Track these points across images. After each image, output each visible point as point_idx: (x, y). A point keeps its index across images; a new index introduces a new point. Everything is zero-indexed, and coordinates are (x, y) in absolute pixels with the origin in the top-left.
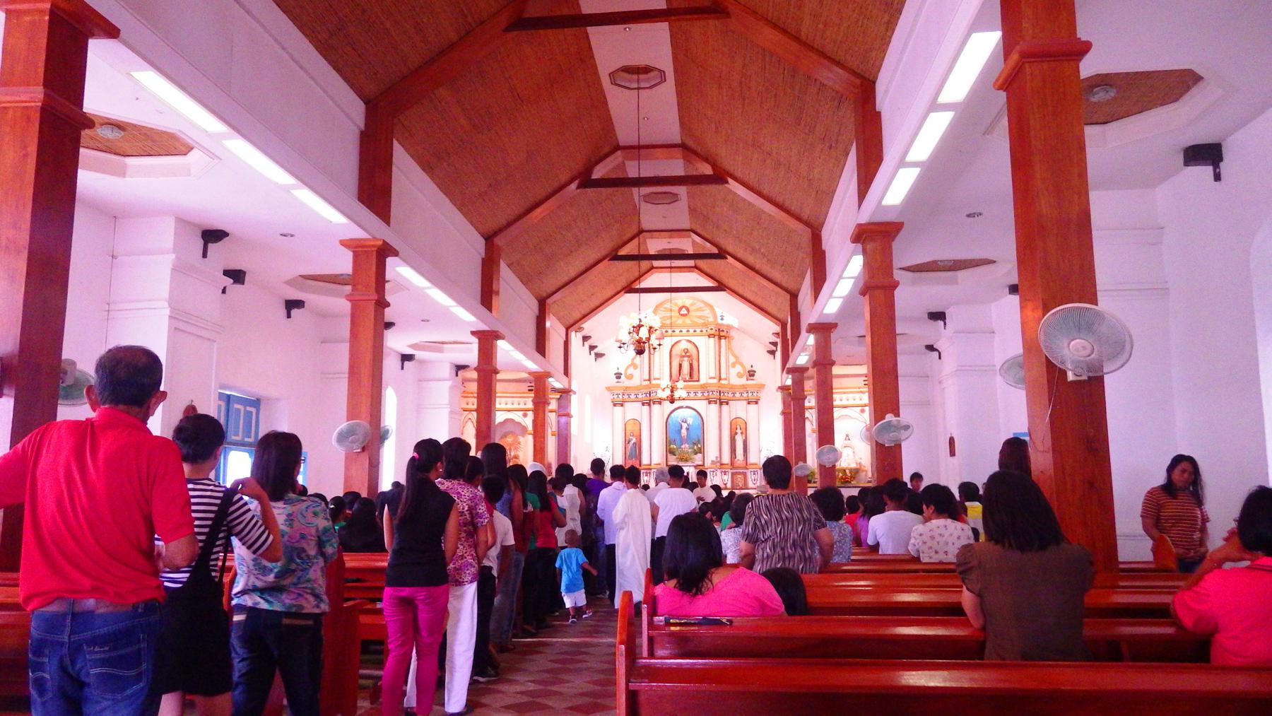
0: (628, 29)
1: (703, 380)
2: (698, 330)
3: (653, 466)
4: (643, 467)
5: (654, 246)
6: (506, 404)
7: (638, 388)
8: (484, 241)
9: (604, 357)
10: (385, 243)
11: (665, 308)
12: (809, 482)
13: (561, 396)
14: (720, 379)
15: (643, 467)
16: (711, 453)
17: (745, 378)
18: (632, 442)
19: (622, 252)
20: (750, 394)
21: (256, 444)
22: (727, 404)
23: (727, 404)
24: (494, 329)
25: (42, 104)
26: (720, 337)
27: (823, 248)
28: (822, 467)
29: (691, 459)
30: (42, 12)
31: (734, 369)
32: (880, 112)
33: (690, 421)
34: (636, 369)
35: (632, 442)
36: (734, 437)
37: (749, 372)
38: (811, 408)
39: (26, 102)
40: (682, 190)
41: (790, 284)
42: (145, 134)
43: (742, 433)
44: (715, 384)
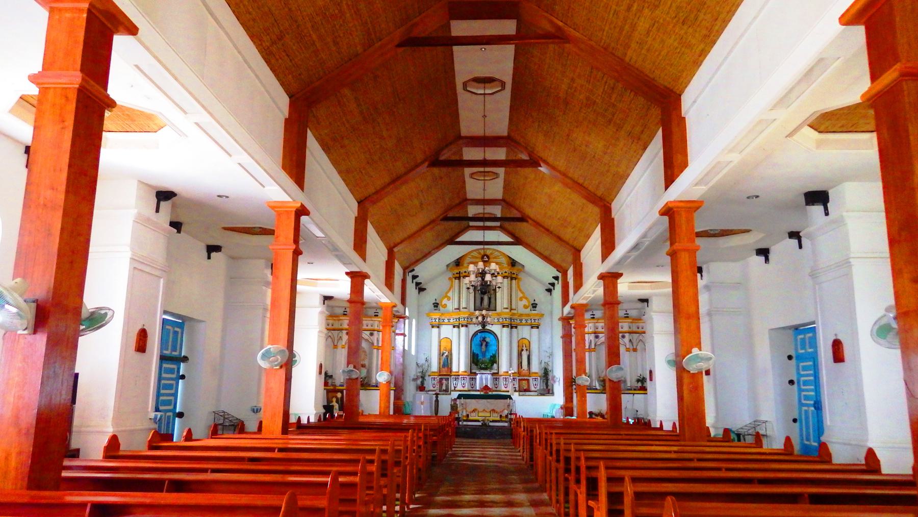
0: (483, 49)
4: (453, 374)
5: (472, 210)
6: (367, 326)
8: (357, 204)
10: (302, 205)
11: (472, 256)
13: (398, 320)
14: (511, 309)
15: (453, 374)
17: (529, 309)
18: (446, 355)
19: (451, 214)
20: (533, 321)
21: (163, 355)
22: (516, 327)
23: (516, 327)
25: (79, 86)
27: (613, 216)
30: (80, 10)
32: (685, 118)
34: (449, 300)
35: (446, 355)
36: (521, 353)
37: (532, 304)
39: (65, 84)
40: (501, 171)
42: (128, 115)
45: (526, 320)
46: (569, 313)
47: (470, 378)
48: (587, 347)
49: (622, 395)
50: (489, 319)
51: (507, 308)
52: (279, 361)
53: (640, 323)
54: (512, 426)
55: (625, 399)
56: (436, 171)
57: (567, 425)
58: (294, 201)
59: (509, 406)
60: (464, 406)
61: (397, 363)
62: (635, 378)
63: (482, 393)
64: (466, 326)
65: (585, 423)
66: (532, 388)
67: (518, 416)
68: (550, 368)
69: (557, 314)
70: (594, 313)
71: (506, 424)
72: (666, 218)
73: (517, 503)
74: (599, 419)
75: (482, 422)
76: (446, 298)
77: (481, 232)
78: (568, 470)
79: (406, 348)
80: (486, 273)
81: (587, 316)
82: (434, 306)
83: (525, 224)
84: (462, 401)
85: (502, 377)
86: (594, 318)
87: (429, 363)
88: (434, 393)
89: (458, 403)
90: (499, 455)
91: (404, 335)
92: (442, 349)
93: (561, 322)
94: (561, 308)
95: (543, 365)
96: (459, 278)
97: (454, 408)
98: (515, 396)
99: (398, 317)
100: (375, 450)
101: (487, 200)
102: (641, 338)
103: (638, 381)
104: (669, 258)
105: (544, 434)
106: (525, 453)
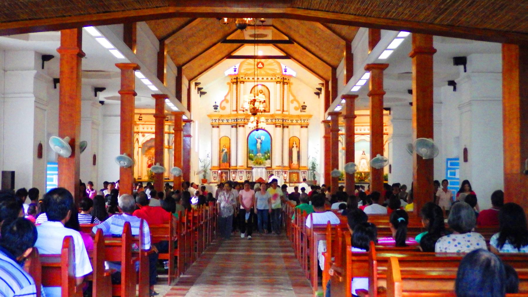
1: (272, 112)
2: (269, 79)
3: (238, 167)
7: (229, 116)
9: (206, 94)
11: (248, 63)
12: (340, 180)
14: (283, 111)
15: (231, 168)
16: (277, 161)
17: (299, 111)
18: (225, 151)
19: (228, 38)
22: (288, 127)
23: (288, 127)
24: (165, 94)
26: (284, 83)
27: (352, 52)
28: (347, 174)
29: (263, 163)
33: (263, 138)
35: (225, 151)
37: (302, 106)
38: (342, 134)
41: (333, 62)
43: (297, 147)
44: (280, 114)
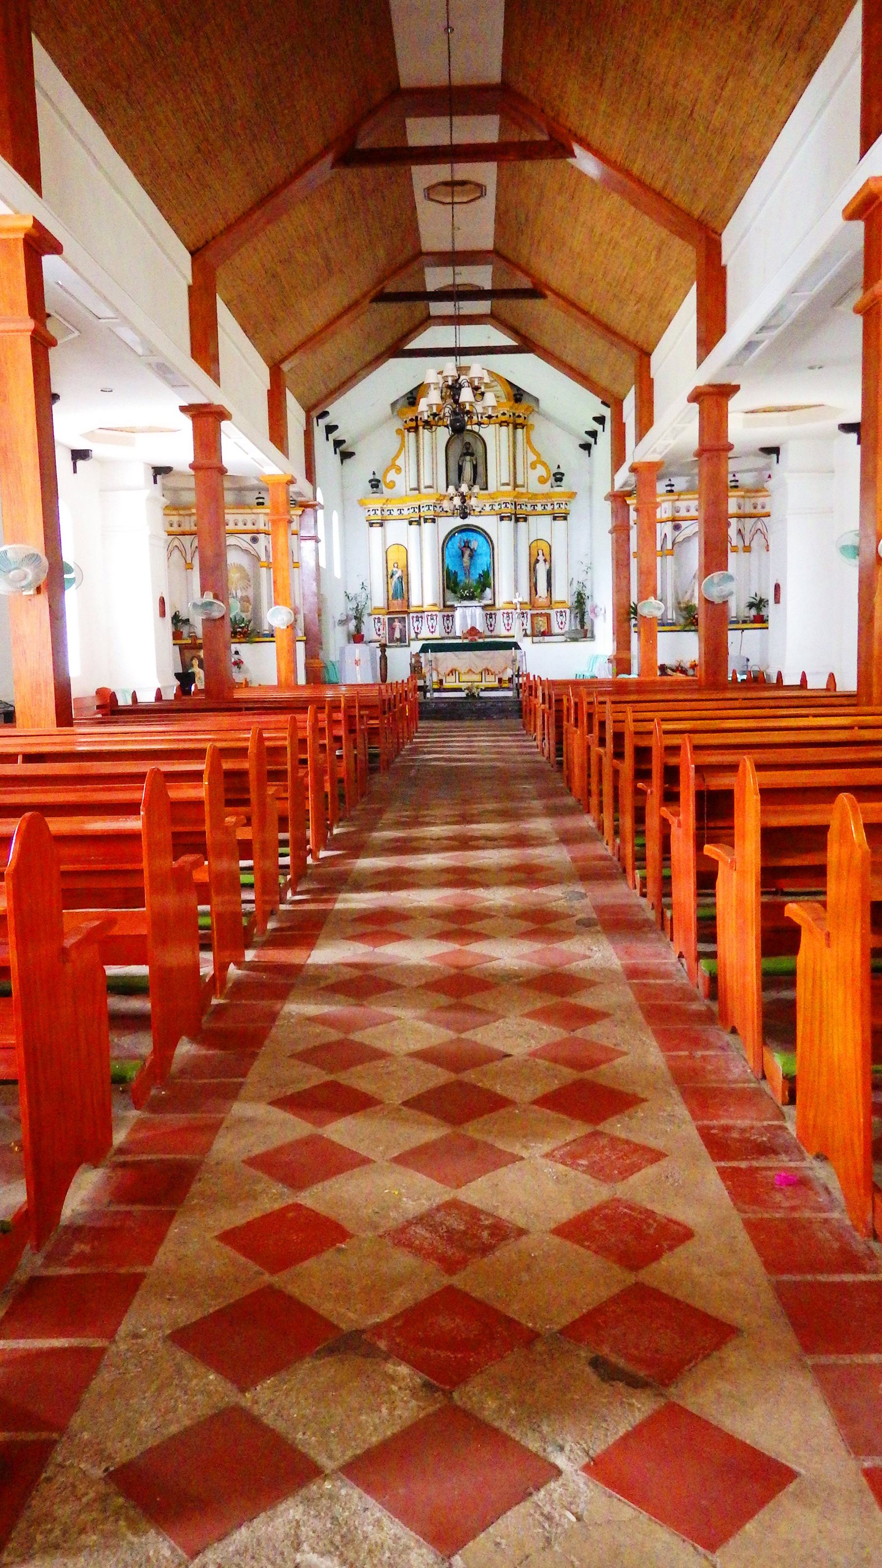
4: (412, 609)
13: (303, 511)
14: (516, 486)
15: (412, 609)
17: (548, 484)
18: (397, 575)
20: (556, 507)
22: (525, 520)
23: (525, 520)
31: (534, 471)
35: (397, 575)
37: (554, 475)
45: (544, 506)
46: (625, 484)
47: (444, 616)
48: (659, 548)
49: (729, 632)
50: (473, 502)
51: (508, 484)
52: (30, 577)
53: (760, 497)
54: (521, 696)
55: (733, 637)
56: (350, 175)
57: (620, 688)
58: (17, 212)
59: (514, 661)
60: (433, 663)
61: (307, 592)
62: (746, 599)
63: (466, 641)
64: (433, 521)
65: (653, 683)
66: (556, 629)
67: (531, 678)
68: (587, 592)
69: (603, 488)
70: (672, 483)
71: (510, 694)
72: (859, 226)
73: (537, 838)
74: (680, 676)
75: (467, 691)
76: (394, 470)
77: (451, 329)
78: (642, 774)
79: (323, 564)
80: (461, 387)
81: (661, 487)
82: (372, 486)
83: (539, 303)
84: (430, 655)
85: (502, 611)
86: (671, 491)
87: (368, 592)
88: (377, 644)
89: (422, 660)
90: (499, 747)
91: (316, 539)
92: (390, 565)
93: (609, 502)
94: (610, 475)
95: (575, 587)
96: (416, 429)
97: (416, 669)
98: (526, 644)
99: (301, 506)
100: (205, 750)
101: (458, 253)
102: (759, 525)
103: (751, 605)
104: (859, 320)
105: (585, 704)
106: (546, 741)
